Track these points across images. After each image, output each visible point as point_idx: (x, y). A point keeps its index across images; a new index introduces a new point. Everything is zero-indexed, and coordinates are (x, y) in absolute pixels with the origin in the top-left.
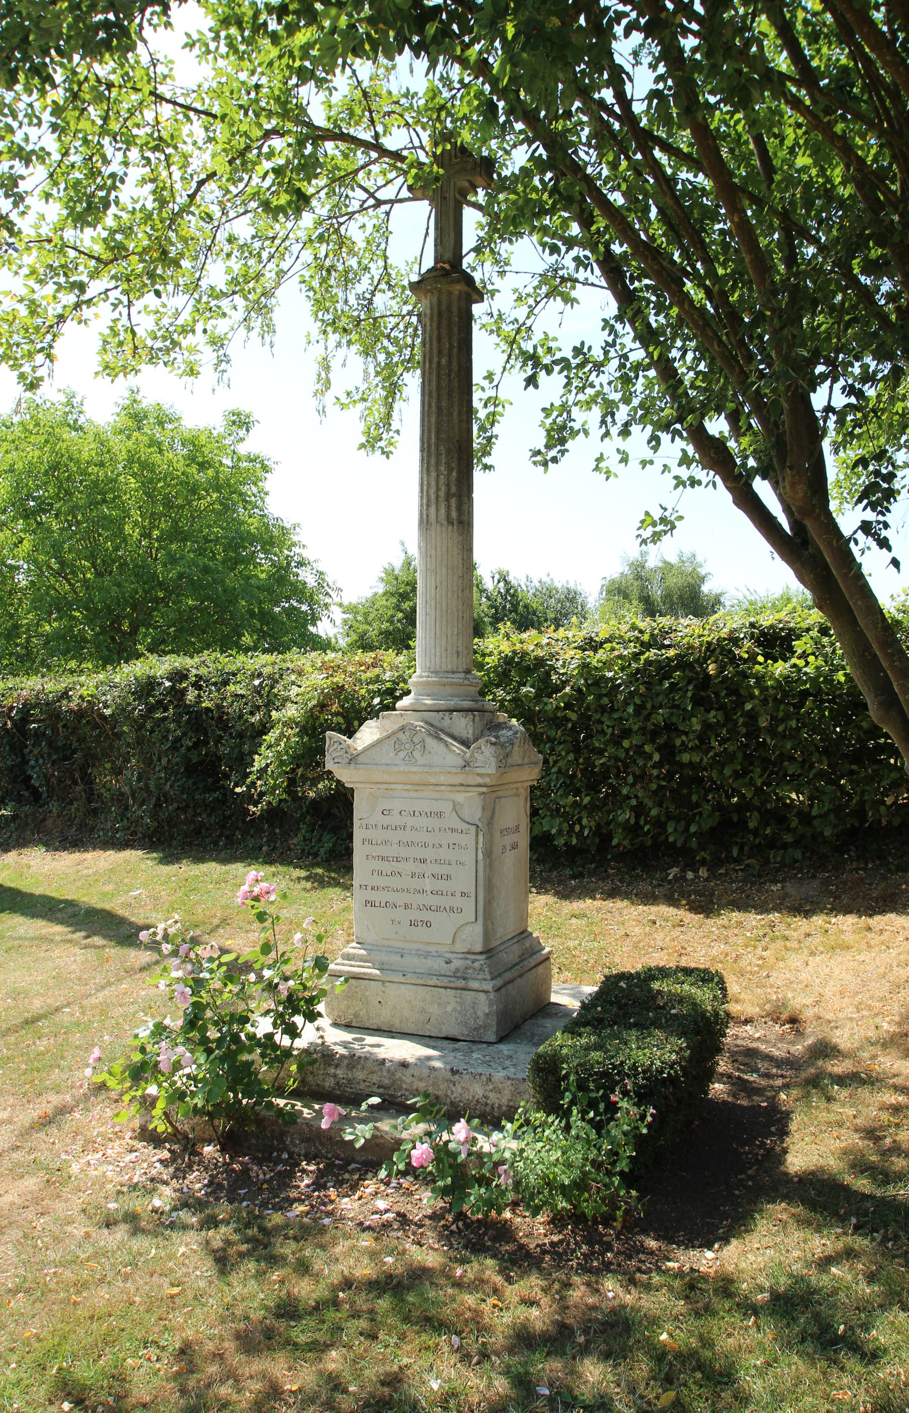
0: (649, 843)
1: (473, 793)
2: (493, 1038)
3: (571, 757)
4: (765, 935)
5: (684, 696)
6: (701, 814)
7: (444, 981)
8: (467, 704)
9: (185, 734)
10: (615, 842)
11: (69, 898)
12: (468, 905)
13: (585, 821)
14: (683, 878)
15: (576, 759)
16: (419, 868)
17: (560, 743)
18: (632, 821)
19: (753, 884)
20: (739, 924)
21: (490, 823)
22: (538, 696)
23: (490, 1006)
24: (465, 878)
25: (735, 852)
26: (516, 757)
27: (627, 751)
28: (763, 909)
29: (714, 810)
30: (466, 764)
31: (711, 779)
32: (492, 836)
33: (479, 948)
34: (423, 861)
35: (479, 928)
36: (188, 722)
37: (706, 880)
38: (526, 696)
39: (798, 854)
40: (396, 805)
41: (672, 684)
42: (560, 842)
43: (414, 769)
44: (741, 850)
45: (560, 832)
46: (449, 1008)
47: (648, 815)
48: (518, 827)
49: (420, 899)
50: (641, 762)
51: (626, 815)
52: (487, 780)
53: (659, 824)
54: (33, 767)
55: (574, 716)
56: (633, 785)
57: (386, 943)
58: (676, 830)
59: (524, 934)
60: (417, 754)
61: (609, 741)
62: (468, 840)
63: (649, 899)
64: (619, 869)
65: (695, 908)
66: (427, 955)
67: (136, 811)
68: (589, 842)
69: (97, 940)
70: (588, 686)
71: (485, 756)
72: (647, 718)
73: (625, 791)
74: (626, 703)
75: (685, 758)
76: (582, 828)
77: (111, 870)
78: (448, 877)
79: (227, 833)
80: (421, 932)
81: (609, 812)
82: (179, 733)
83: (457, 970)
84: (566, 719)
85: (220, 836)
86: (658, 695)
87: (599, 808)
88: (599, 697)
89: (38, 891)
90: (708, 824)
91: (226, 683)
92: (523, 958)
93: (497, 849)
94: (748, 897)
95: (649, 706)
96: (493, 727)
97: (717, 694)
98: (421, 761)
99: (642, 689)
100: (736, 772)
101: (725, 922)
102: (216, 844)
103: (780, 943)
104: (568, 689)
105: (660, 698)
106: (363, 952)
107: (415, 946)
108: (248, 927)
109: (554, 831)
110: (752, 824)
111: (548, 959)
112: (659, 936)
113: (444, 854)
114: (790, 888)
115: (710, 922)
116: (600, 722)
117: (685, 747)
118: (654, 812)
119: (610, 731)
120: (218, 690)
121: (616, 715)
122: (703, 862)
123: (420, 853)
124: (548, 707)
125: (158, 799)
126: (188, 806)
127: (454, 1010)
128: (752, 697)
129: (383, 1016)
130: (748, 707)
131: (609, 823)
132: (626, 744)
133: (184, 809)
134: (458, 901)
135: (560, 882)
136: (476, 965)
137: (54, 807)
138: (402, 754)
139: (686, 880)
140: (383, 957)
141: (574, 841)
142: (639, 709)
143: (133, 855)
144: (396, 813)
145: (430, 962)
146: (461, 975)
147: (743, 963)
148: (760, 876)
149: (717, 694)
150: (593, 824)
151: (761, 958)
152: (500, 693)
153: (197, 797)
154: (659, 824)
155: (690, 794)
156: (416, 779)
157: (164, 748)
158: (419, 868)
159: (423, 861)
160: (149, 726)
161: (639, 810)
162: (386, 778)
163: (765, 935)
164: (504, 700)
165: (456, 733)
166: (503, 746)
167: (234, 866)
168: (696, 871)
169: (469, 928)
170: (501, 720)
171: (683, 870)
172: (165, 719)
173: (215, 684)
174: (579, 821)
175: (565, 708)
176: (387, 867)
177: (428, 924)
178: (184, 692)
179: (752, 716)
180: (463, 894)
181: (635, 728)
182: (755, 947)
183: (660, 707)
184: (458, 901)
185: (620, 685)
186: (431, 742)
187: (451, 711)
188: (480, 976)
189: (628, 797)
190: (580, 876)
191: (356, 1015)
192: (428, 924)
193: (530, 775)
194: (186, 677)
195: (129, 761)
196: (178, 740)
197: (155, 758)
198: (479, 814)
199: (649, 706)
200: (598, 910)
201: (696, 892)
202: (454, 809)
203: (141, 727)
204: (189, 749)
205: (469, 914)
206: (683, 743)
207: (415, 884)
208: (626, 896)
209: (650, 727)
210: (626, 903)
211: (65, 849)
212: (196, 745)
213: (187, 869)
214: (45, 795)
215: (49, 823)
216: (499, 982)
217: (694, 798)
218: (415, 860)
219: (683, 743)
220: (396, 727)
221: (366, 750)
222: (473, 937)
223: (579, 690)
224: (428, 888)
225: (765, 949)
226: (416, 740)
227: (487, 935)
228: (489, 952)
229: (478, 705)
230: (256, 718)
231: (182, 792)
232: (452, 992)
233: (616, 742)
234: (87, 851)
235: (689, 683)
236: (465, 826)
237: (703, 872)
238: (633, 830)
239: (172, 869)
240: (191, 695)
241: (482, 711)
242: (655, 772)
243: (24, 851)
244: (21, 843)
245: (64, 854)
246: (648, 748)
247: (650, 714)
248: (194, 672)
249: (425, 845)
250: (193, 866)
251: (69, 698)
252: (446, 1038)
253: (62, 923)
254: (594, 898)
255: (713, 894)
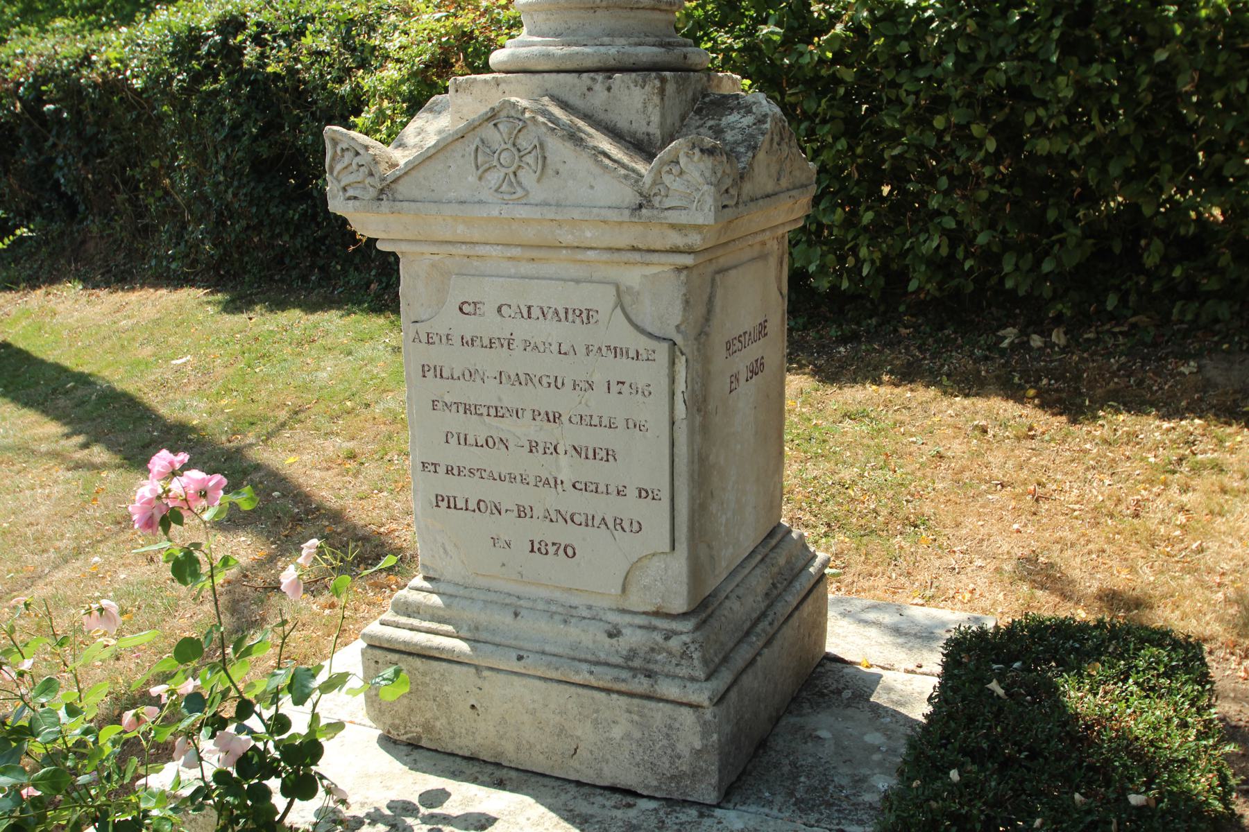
0: (971, 287)
1: (662, 267)
2: (711, 797)
3: (842, 144)
4: (1181, 460)
5: (1044, 39)
6: (1062, 242)
7: (605, 677)
8: (647, 53)
9: (246, 115)
10: (913, 286)
11: (86, 369)
12: (655, 517)
13: (863, 252)
14: (1024, 345)
15: (851, 148)
16: (544, 433)
17: (824, 122)
18: (944, 251)
19: (1145, 359)
20: (1132, 437)
21: (702, 334)
22: (787, 42)
23: (705, 734)
24: (645, 459)
25: (1111, 302)
26: (762, 179)
27: (940, 135)
28: (1171, 410)
29: (1086, 236)
30: (644, 203)
31: (1084, 183)
32: (706, 360)
33: (679, 604)
34: (554, 418)
35: (679, 565)
36: (250, 97)
37: (1063, 350)
38: (768, 41)
39: (1224, 310)
40: (490, 292)
41: (1024, 16)
42: (824, 285)
43: (522, 212)
44: (1124, 300)
45: (822, 269)
46: (617, 732)
47: (971, 242)
48: (763, 326)
49: (549, 499)
50: (963, 154)
51: (933, 243)
52: (695, 240)
53: (990, 258)
54: (61, 168)
55: (848, 74)
56: (947, 193)
57: (481, 582)
58: (1017, 268)
59: (776, 535)
60: (528, 177)
61: (909, 117)
62: (652, 373)
63: (970, 385)
64: (916, 328)
65: (1048, 403)
66: (568, 615)
67: (197, 231)
68: (867, 283)
69: (99, 454)
70: (874, 20)
71: (689, 181)
72: (978, 77)
73: (934, 204)
74: (941, 51)
75: (1043, 146)
76: (859, 263)
77: (157, 322)
78: (610, 455)
79: (321, 262)
80: (552, 568)
81: (905, 236)
82: (236, 114)
83: (632, 654)
84: (837, 80)
85: (312, 267)
86: (998, 35)
87: (888, 231)
88: (894, 40)
89: (51, 356)
90: (1072, 260)
91: (301, 33)
92: (772, 597)
93: (719, 386)
94: (1140, 383)
95: (981, 55)
96: (712, 106)
97: (1105, 36)
98: (538, 194)
99: (971, 26)
100: (1126, 170)
101: (1106, 432)
102: (305, 278)
103: (1210, 479)
104: (839, 28)
105: (1002, 42)
106: (435, 600)
107: (543, 593)
108: (327, 427)
109: (812, 268)
110: (1150, 260)
111: (822, 577)
112: (995, 458)
113: (599, 403)
114: (1214, 371)
115: (1081, 430)
116: (894, 85)
117: (1041, 129)
118: (982, 239)
119: (911, 100)
120: (289, 46)
121: (922, 73)
122: (1059, 320)
123: (547, 400)
124: (806, 60)
125: (220, 214)
126: (261, 223)
127: (628, 736)
128: (1166, 38)
129: (479, 735)
130: (1161, 56)
131: (903, 254)
132: (939, 122)
133: (257, 229)
134: (631, 508)
135: (822, 349)
136: (674, 644)
137: (94, 225)
138: (494, 177)
139: (1030, 349)
140: (474, 614)
141: (845, 284)
142: (964, 60)
143: (191, 296)
144: (489, 309)
145: (575, 633)
146: (641, 666)
147: (1152, 520)
148: (1155, 345)
149: (1105, 36)
150: (877, 255)
151: (1182, 509)
152: (724, 38)
153: (273, 210)
154: (990, 258)
155: (1044, 209)
156: (529, 234)
157: (220, 137)
158: (544, 433)
159: (554, 418)
160: (195, 103)
161: (955, 237)
162: (461, 231)
163: (1181, 460)
164: (731, 48)
165: (622, 124)
166: (731, 154)
167: (326, 316)
168: (1045, 334)
169: (656, 565)
170: (726, 89)
171: (1024, 332)
172: (216, 93)
173: (284, 36)
174: (854, 250)
175: (834, 61)
176: (478, 428)
177: (569, 552)
178: (240, 50)
179: (1166, 74)
180: (642, 493)
181: (956, 94)
182: (1166, 484)
183: (1002, 57)
184: (631, 508)
185: (931, 20)
186: (558, 149)
187: (609, 70)
188: (683, 671)
189: (938, 213)
190: (853, 338)
191: (428, 728)
192: (569, 552)
193: (791, 211)
194: (242, 26)
195: (176, 158)
196: (236, 125)
197: (210, 150)
198: (675, 315)
199: (981, 55)
200: (887, 404)
201: (1049, 373)
202: (620, 303)
203: (186, 105)
204: (255, 139)
205: (657, 533)
206: (1038, 121)
207: (537, 465)
208: (932, 379)
209: (983, 91)
210: (932, 392)
211: (108, 285)
212: (264, 132)
213: (262, 322)
214: (82, 208)
215: (91, 246)
216: (720, 683)
217: (1052, 215)
218: (535, 414)
219: (1038, 121)
220: (484, 109)
221: (413, 167)
222: (669, 583)
223: (858, 29)
224: (566, 475)
225: (1185, 489)
226: (523, 143)
227: (696, 572)
228: (702, 609)
229: (674, 56)
230: (345, 88)
231: (251, 203)
232: (623, 701)
233: (922, 119)
234: (133, 289)
235: (1054, 15)
236: (643, 343)
237: (1058, 337)
238: (943, 266)
239: (240, 319)
240: (251, 54)
241: (683, 68)
242: (987, 171)
243: (54, 289)
244: (53, 278)
245: (103, 293)
246: (976, 130)
247: (982, 71)
248: (253, 18)
249: (557, 384)
250: (268, 316)
251: (91, 65)
252: (613, 789)
253: (57, 418)
254: (877, 382)
255: (1078, 378)
